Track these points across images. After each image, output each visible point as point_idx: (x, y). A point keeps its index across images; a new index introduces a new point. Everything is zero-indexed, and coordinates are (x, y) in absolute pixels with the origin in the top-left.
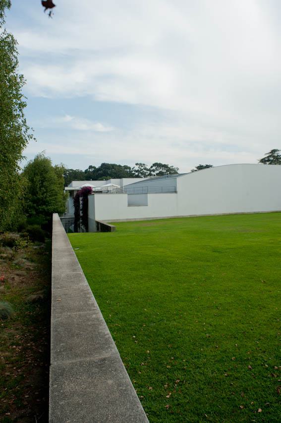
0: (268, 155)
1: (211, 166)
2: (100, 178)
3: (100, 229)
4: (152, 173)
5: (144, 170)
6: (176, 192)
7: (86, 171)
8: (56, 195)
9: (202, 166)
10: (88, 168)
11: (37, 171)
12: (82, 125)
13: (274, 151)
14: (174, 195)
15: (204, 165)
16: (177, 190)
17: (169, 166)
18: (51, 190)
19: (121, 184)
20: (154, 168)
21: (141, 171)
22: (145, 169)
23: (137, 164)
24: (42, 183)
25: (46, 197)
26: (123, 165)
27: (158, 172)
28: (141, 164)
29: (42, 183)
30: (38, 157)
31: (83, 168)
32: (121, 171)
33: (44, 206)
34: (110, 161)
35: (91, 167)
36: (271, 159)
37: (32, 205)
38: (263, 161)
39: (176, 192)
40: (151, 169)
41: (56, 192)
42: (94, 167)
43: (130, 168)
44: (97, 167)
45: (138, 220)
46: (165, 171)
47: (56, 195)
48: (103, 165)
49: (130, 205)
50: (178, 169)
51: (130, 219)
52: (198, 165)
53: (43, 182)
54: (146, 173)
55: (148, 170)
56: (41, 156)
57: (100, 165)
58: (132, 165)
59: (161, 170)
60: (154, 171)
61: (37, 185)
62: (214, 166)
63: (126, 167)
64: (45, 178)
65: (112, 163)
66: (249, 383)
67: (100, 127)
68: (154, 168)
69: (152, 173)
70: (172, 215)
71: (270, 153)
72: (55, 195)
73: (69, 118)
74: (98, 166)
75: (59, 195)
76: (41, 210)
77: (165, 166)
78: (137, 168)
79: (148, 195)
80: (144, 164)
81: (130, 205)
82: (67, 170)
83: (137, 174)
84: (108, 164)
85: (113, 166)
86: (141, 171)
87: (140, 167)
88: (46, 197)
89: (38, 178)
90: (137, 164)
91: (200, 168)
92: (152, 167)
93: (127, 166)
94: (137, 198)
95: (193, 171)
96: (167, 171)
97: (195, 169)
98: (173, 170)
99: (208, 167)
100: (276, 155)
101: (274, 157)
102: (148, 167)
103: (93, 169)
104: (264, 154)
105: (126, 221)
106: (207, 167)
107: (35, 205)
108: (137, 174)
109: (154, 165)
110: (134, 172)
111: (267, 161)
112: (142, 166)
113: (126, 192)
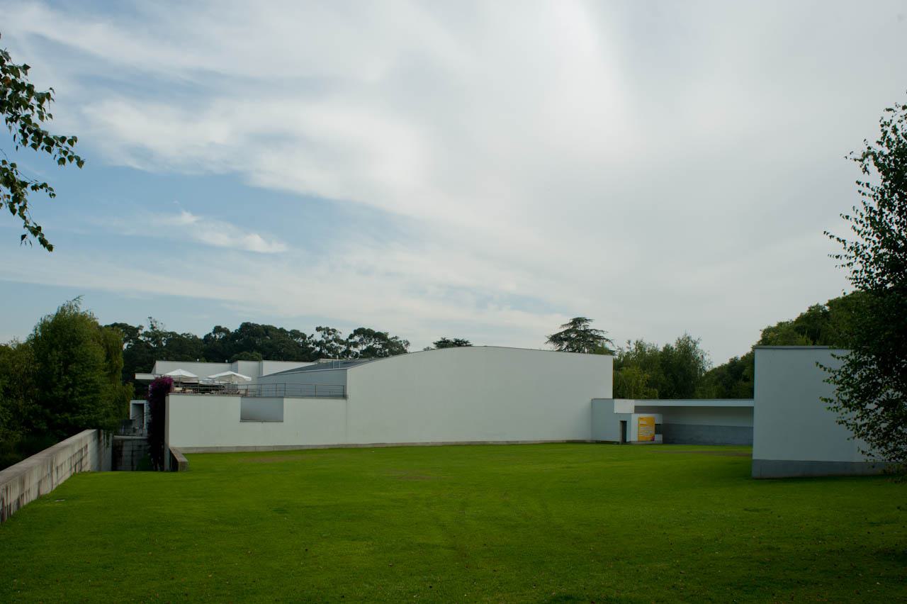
0: (566, 328)
3: (135, 467)
4: (352, 349)
5: (333, 343)
6: (344, 396)
7: (208, 337)
8: (97, 392)
9: (448, 341)
10: (211, 331)
11: (56, 340)
12: (218, 235)
13: (577, 321)
14: (341, 402)
15: (451, 338)
16: (348, 392)
17: (389, 337)
18: (84, 382)
19: (260, 370)
20: (357, 338)
21: (328, 345)
22: (337, 340)
23: (318, 329)
24: (66, 366)
25: (72, 395)
26: (288, 329)
27: (364, 347)
28: (328, 329)
29: (66, 366)
30: (63, 309)
31: (200, 330)
32: (284, 342)
33: (67, 415)
34: (260, 318)
35: (218, 329)
36: (573, 335)
38: (556, 339)
39: (344, 396)
40: (350, 341)
41: (96, 386)
43: (304, 336)
44: (232, 330)
45: (262, 450)
46: (380, 346)
47: (97, 392)
48: (246, 327)
49: (245, 418)
50: (408, 344)
51: (245, 447)
52: (440, 340)
53: (67, 363)
54: (336, 348)
55: (342, 342)
56: (71, 307)
57: (238, 327)
58: (308, 330)
59: (371, 344)
60: (355, 344)
61: (54, 370)
63: (296, 334)
64: (73, 356)
65: (266, 324)
67: (256, 242)
68: (357, 338)
69: (352, 349)
70: (336, 443)
71: (571, 324)
72: (93, 392)
73: (187, 218)
74: (233, 327)
75: (103, 391)
76: (59, 421)
77: (380, 336)
78: (318, 337)
79: (285, 400)
80: (334, 331)
81: (245, 418)
82: (165, 334)
83: (318, 349)
84: (257, 326)
85: (267, 330)
86: (328, 345)
87: (326, 335)
88: (72, 395)
89: (56, 354)
90: (318, 329)
91: (443, 344)
92: (351, 337)
93: (298, 331)
94: (255, 404)
95: (427, 349)
96: (385, 346)
97: (433, 346)
98: (398, 345)
100: (582, 329)
101: (577, 332)
102: (344, 337)
103: (224, 334)
104: (560, 326)
105: (234, 450)
106: (459, 343)
107: (48, 411)
108: (318, 349)
109: (358, 332)
110: (311, 346)
111: (566, 340)
112: (329, 334)
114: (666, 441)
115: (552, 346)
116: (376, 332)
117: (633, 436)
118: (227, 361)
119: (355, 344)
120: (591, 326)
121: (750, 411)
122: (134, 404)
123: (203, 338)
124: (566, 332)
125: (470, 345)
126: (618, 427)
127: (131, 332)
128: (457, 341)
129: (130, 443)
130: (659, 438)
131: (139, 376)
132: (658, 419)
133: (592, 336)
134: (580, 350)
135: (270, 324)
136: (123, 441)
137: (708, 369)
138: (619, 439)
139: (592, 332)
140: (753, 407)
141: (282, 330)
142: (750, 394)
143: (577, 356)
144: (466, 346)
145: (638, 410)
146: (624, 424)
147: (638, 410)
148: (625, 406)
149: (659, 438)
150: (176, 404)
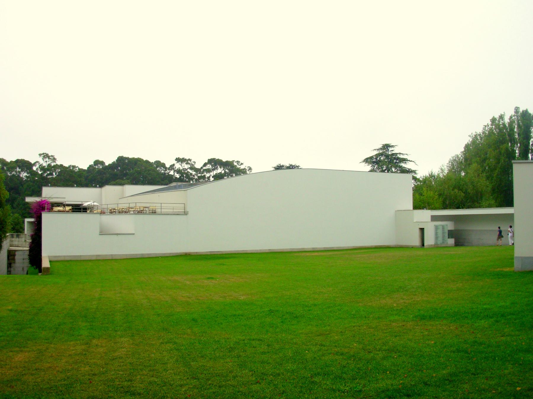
0: (376, 152)
1: (298, 167)
2: (113, 182)
6: (185, 213)
13: (386, 147)
20: (209, 166)
34: (130, 154)
37: (223, 172)
39: (185, 213)
42: (102, 163)
43: (163, 165)
48: (121, 160)
49: (102, 233)
60: (208, 171)
62: (302, 166)
63: (159, 164)
66: (99, 349)
71: (381, 149)
81: (102, 233)
91: (279, 168)
92: (205, 165)
99: (292, 168)
101: (387, 156)
102: (198, 166)
106: (291, 167)
109: (211, 161)
113: (507, 171)
114: (458, 244)
115: (368, 168)
116: (144, 160)
117: (429, 240)
118: (98, 186)
119: (208, 171)
120: (396, 150)
121: (510, 217)
122: (28, 222)
123: (86, 169)
124: (377, 155)
125: (244, 172)
126: (417, 233)
127: (24, 165)
128: (291, 165)
129: (20, 253)
130: (451, 241)
131: (28, 200)
132: (450, 226)
133: (398, 159)
134: (389, 170)
135: (23, 158)
136: (15, 251)
137: (42, 212)
138: (417, 243)
139: (398, 155)
140: (424, 228)
141: (147, 162)
142: (509, 203)
143: (386, 175)
144: (298, 168)
145: (434, 218)
146: (422, 230)
147: (434, 218)
148: (425, 215)
149: (451, 241)
150: (46, 217)
